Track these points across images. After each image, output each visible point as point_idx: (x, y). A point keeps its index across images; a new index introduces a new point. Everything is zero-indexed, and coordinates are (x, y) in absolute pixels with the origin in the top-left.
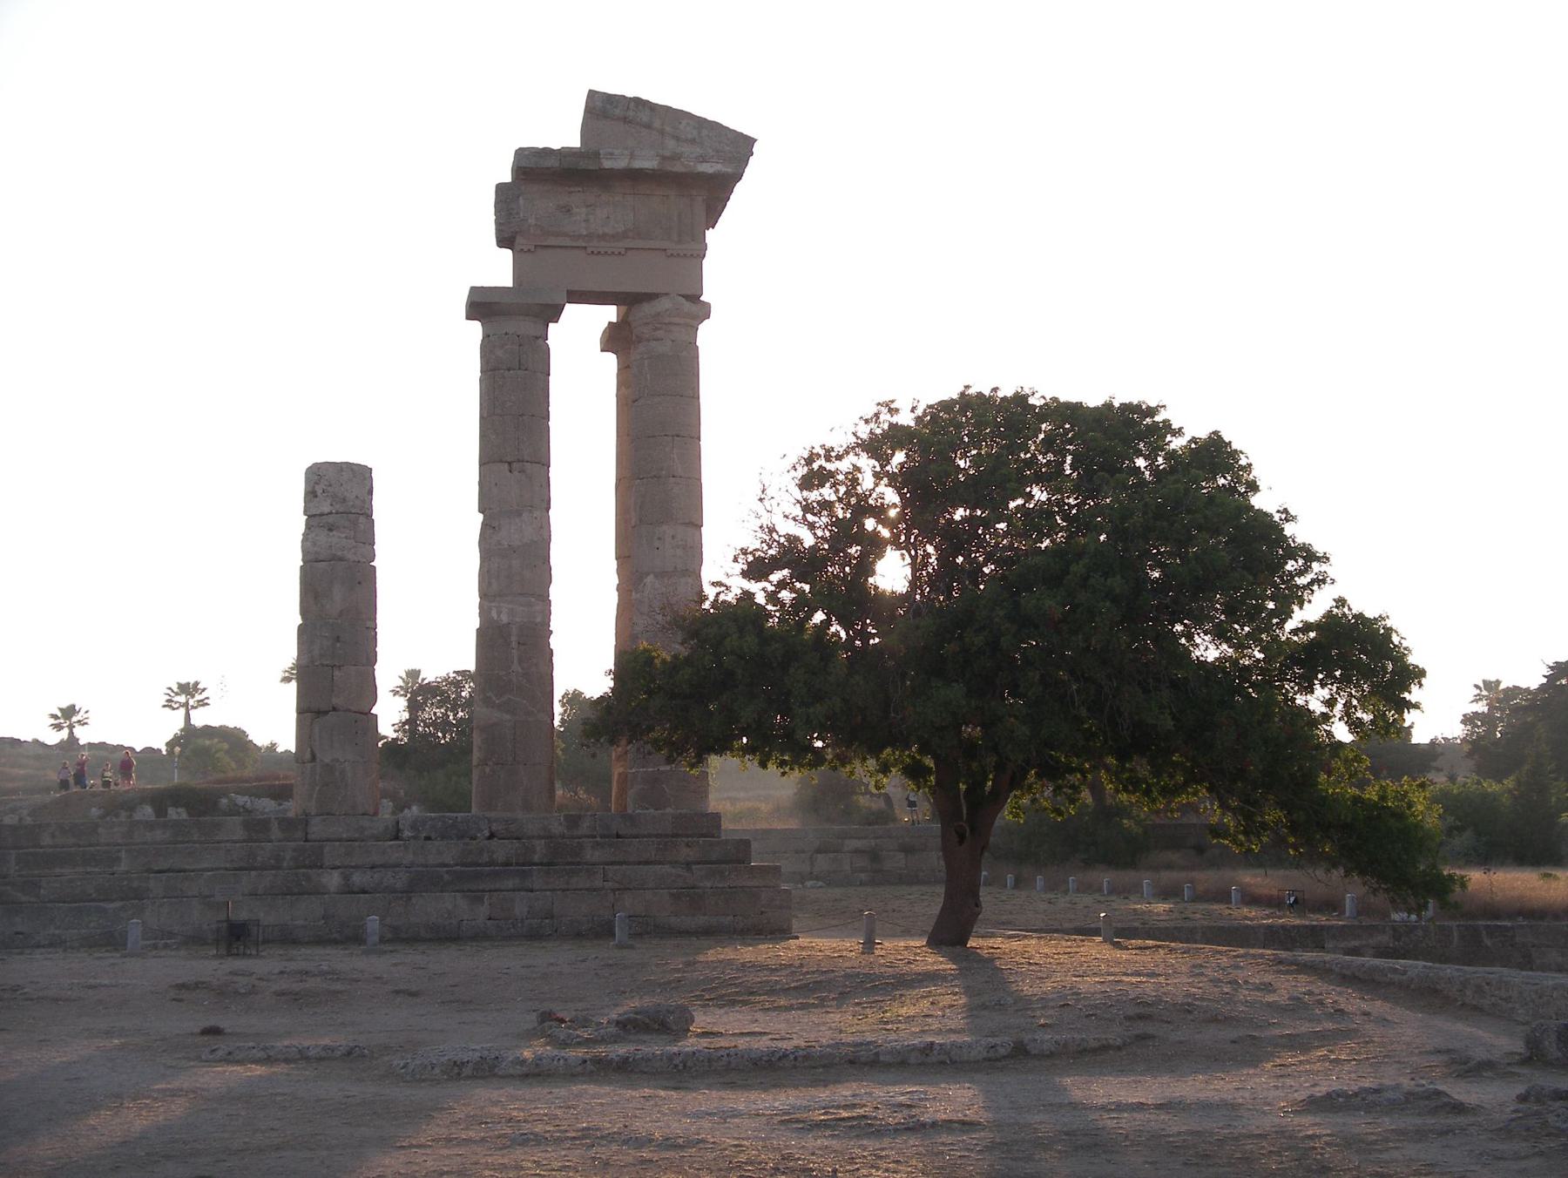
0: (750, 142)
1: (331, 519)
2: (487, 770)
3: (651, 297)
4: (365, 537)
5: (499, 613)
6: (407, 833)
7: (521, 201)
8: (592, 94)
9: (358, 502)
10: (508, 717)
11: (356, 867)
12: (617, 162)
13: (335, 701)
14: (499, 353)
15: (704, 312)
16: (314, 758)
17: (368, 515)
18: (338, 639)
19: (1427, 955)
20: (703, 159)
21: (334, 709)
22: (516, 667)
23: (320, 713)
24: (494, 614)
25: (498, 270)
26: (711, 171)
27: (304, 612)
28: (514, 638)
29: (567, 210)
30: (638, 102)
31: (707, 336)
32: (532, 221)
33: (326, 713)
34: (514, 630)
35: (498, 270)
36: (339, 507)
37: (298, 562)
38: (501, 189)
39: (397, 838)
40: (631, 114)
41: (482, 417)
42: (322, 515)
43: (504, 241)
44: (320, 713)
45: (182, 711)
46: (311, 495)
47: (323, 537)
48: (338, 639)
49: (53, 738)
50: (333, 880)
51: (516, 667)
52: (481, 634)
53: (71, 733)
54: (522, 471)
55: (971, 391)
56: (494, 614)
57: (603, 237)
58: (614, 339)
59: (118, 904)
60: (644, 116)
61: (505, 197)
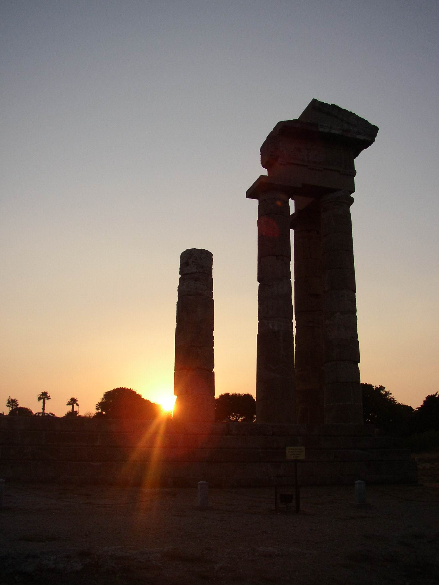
36: (196, 269)
42: (192, 273)
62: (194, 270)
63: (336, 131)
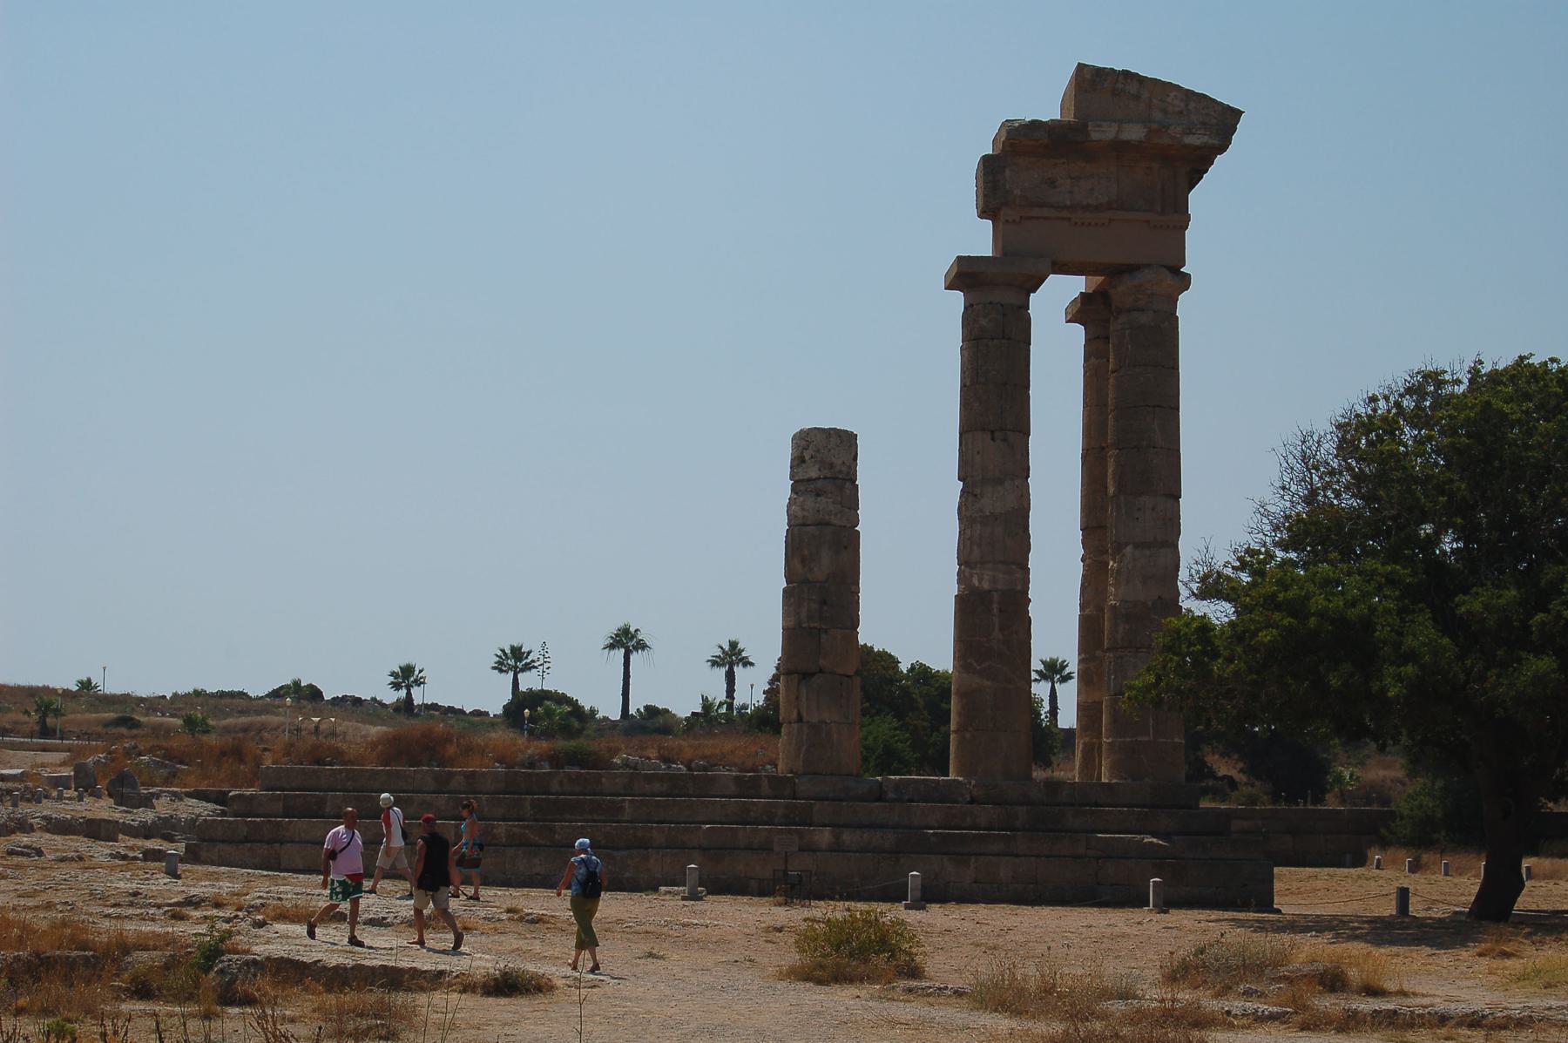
0: (1237, 114)
1: (819, 484)
2: (968, 736)
3: (1132, 269)
4: (850, 502)
5: (980, 580)
6: (891, 795)
7: (1008, 172)
8: (1081, 67)
9: (844, 469)
10: (988, 683)
11: (846, 826)
12: (1103, 133)
13: (822, 662)
14: (983, 322)
15: (1185, 282)
16: (800, 719)
17: (852, 479)
18: (824, 602)
19: (213, 864)
20: (1189, 131)
21: (821, 671)
22: (996, 634)
23: (806, 676)
24: (976, 582)
25: (980, 239)
26: (1198, 142)
27: (790, 575)
28: (995, 606)
29: (1052, 183)
30: (1126, 73)
31: (1186, 305)
32: (1017, 192)
33: (813, 674)
34: (996, 596)
35: (980, 239)
36: (825, 474)
37: (783, 526)
38: (986, 161)
39: (879, 799)
40: (1119, 86)
41: (963, 386)
42: (809, 480)
43: (987, 210)
44: (806, 676)
45: (511, 674)
46: (798, 461)
47: (810, 503)
48: (824, 602)
49: (390, 697)
50: (824, 836)
51: (996, 634)
52: (961, 600)
53: (409, 694)
54: (1005, 440)
55: (1486, 368)
56: (976, 582)
57: (1086, 208)
58: (1082, 311)
59: (625, 853)
60: (1133, 88)
61: (990, 169)
62: (814, 473)
63: (1134, 133)
